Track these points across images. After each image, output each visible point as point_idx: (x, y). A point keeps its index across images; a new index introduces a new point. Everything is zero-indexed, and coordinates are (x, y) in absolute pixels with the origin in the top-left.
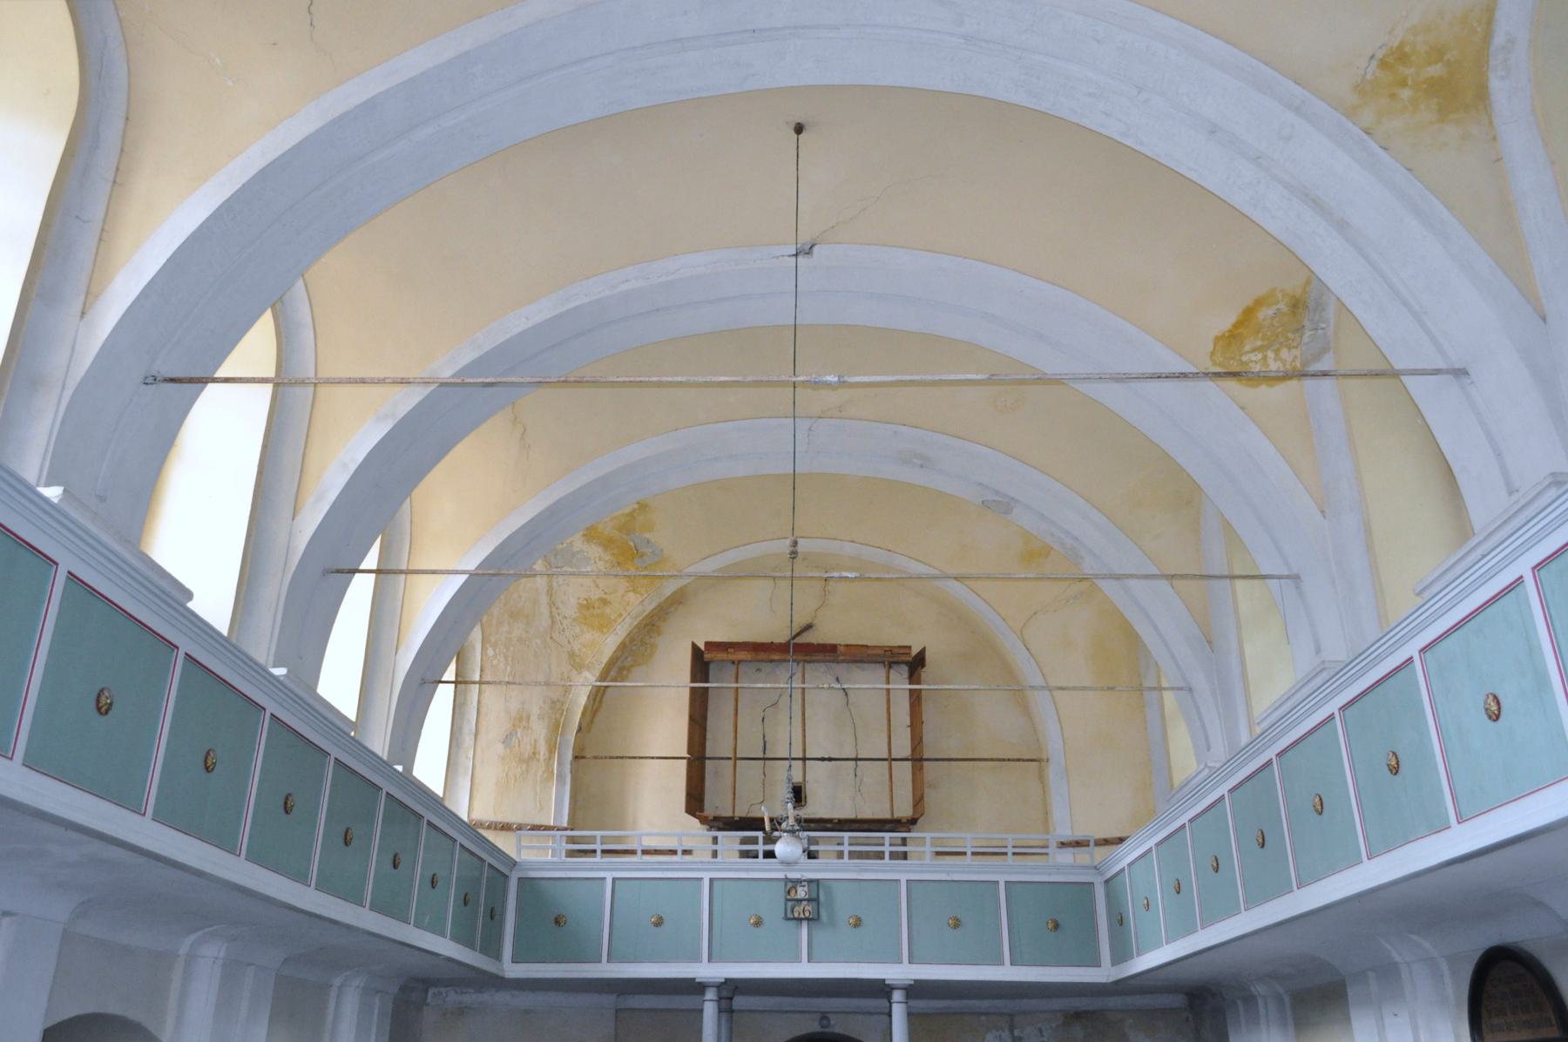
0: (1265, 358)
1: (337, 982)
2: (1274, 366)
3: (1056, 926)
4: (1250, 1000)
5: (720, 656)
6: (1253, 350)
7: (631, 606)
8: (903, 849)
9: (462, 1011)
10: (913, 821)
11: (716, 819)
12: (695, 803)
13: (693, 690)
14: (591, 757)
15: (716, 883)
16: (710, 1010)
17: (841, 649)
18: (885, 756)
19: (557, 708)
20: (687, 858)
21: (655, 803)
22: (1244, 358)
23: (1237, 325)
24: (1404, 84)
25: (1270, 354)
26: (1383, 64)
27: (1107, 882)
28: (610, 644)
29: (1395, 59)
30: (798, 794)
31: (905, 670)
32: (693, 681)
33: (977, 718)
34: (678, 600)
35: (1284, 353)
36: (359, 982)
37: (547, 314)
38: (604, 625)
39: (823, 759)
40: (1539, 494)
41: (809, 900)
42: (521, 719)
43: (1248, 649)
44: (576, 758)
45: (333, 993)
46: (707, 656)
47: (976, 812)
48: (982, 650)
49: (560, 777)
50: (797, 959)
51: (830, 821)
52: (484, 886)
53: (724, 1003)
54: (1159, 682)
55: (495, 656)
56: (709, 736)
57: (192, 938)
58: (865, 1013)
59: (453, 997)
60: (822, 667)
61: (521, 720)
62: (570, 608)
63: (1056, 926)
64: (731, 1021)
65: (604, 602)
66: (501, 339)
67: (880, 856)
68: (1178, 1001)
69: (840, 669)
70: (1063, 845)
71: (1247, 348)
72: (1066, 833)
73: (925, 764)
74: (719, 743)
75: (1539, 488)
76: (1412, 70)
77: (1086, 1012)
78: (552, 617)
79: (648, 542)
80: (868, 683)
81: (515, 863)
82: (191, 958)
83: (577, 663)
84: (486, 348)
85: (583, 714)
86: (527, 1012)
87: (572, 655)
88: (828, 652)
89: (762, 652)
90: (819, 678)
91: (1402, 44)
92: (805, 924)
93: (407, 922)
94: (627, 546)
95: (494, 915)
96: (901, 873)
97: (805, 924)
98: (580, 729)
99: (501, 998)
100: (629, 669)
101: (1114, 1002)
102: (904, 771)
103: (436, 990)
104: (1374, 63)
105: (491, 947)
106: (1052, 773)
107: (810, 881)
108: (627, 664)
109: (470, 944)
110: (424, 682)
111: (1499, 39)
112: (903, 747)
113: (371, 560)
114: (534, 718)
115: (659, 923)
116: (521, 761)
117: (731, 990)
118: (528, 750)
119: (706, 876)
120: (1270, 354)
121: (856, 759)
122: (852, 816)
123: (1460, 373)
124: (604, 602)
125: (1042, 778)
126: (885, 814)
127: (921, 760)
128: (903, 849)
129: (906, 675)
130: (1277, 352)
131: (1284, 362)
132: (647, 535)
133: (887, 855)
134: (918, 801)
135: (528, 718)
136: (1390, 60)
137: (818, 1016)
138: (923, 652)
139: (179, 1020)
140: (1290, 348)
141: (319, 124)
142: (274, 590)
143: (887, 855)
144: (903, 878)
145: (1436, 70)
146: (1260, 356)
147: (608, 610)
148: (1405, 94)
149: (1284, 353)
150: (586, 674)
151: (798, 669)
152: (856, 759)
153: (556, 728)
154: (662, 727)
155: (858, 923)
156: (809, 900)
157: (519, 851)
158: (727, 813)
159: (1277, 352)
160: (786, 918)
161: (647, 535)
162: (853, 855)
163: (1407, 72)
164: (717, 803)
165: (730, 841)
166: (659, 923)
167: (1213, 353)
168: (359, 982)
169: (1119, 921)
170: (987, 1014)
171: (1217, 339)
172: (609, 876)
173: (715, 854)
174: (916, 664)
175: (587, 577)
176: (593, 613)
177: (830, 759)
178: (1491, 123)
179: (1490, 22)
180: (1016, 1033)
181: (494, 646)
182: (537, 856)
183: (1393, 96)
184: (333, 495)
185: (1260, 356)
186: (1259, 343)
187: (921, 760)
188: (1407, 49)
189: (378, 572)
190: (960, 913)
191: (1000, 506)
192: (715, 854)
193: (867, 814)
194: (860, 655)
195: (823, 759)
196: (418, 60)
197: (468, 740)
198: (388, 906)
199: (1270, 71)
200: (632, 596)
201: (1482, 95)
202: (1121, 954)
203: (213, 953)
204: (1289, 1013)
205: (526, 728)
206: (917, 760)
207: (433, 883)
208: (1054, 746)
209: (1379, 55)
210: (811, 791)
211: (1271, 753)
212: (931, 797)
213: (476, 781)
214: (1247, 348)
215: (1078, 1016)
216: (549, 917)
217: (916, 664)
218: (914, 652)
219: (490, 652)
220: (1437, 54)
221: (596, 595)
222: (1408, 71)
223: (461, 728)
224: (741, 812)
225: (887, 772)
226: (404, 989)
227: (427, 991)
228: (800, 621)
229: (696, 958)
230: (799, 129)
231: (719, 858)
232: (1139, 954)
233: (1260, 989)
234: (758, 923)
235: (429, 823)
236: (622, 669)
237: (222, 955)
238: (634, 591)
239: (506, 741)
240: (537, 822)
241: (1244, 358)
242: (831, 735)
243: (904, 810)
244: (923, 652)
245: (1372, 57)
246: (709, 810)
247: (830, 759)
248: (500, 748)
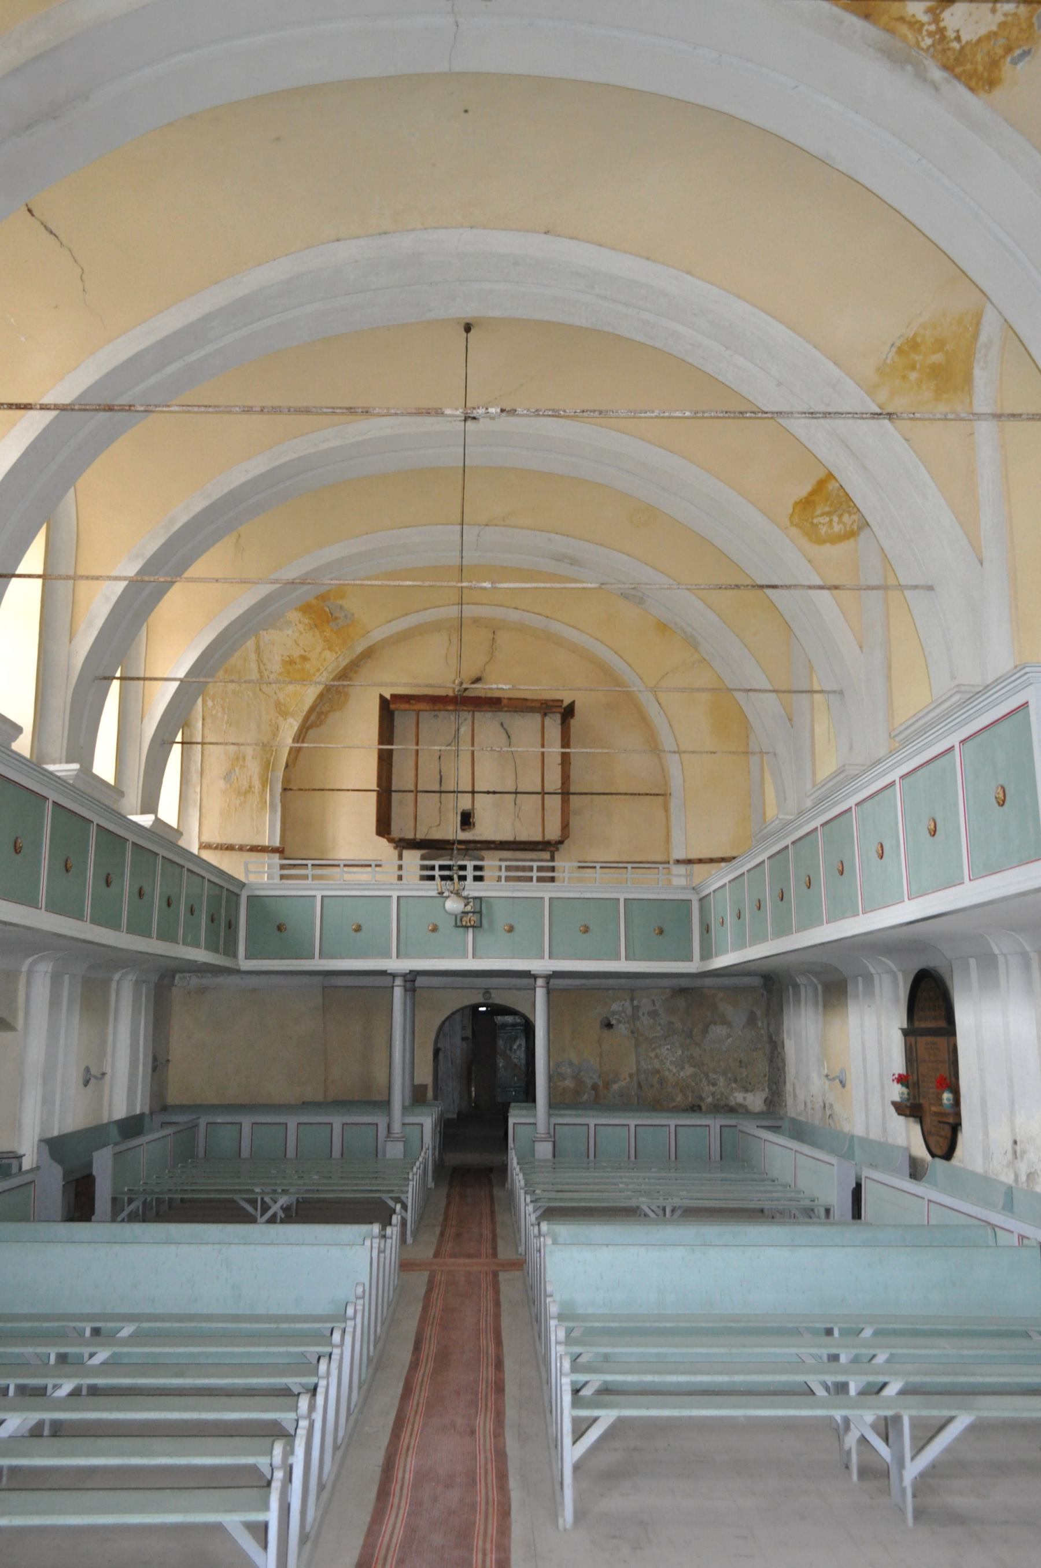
0: (831, 520)
1: (117, 976)
2: (837, 528)
3: (661, 932)
4: (796, 986)
5: (403, 706)
6: (822, 515)
7: (327, 663)
8: (551, 874)
9: (203, 990)
10: (561, 842)
11: (401, 840)
12: (383, 827)
13: (380, 751)
14: (297, 787)
15: (402, 900)
16: (398, 992)
17: (505, 702)
18: (539, 790)
19: (267, 749)
20: (377, 869)
21: (350, 825)
22: (815, 521)
23: (813, 493)
24: (913, 368)
25: (835, 518)
26: (900, 351)
27: (700, 900)
28: (310, 694)
29: (910, 347)
30: (467, 820)
31: (558, 718)
32: (381, 742)
33: (614, 756)
34: (368, 654)
35: (846, 518)
36: (131, 977)
37: (262, 469)
38: (304, 679)
39: (488, 793)
40: (951, 696)
41: (474, 913)
42: (238, 759)
43: (816, 726)
44: (285, 790)
45: (114, 985)
46: (392, 706)
47: (612, 830)
48: (624, 702)
49: (273, 806)
50: (465, 956)
51: (493, 842)
52: (221, 907)
53: (408, 985)
54: (668, 853)
55: (214, 706)
56: (394, 770)
57: (30, 960)
58: (517, 989)
59: (195, 981)
60: (490, 715)
61: (238, 760)
62: (275, 665)
63: (661, 932)
64: (413, 999)
65: (304, 659)
66: (226, 490)
67: (530, 879)
68: (757, 981)
69: (504, 717)
70: (678, 862)
71: (818, 512)
72: (682, 855)
73: (571, 797)
74: (402, 778)
75: (949, 694)
76: (921, 357)
77: (688, 989)
78: (260, 672)
79: (341, 607)
80: (526, 726)
81: (243, 885)
82: (30, 973)
83: (282, 711)
84: (214, 498)
85: (289, 753)
86: (254, 990)
87: (278, 704)
88: (493, 704)
89: (437, 702)
90: (488, 727)
91: (915, 336)
92: (471, 930)
93: (177, 942)
94: (324, 611)
95: (231, 926)
96: (546, 892)
97: (471, 930)
98: (287, 766)
99: (234, 979)
100: (326, 714)
101: (708, 982)
102: (554, 803)
103: (181, 975)
104: (894, 349)
105: (231, 951)
106: (673, 804)
107: (475, 898)
108: (324, 709)
109: (216, 950)
110: (163, 743)
111: (983, 338)
112: (554, 782)
113: (179, 738)
114: (249, 758)
115: (358, 929)
116: (239, 793)
117: (411, 978)
118: (244, 784)
119: (395, 894)
120: (835, 518)
121: (516, 793)
122: (511, 839)
123: (930, 588)
124: (304, 659)
125: (666, 809)
126: (538, 838)
127: (569, 793)
128: (551, 874)
129: (559, 721)
130: (840, 516)
131: (845, 525)
132: (340, 602)
133: (535, 879)
134: (565, 826)
135: (244, 758)
136: (906, 348)
137: (482, 992)
138: (573, 704)
139: (27, 1015)
140: (850, 513)
141: (97, 377)
142: (61, 700)
143: (535, 879)
144: (547, 896)
145: (937, 358)
146: (827, 519)
147: (307, 666)
148: (913, 376)
149: (846, 518)
150: (291, 720)
151: (468, 715)
152: (516, 793)
153: (267, 767)
154: (354, 763)
155: (511, 929)
156: (474, 913)
157: (247, 875)
158: (410, 836)
159: (840, 516)
160: (456, 926)
161: (340, 602)
162: (508, 879)
163: (917, 358)
164: (402, 827)
165: (413, 859)
166: (358, 929)
167: (792, 516)
168: (131, 977)
169: (706, 929)
170: (614, 989)
171: (796, 504)
172: (319, 894)
173: (400, 878)
174: (568, 713)
175: (288, 638)
176: (295, 668)
177: (494, 793)
178: (971, 403)
179: (978, 324)
180: (635, 1003)
181: (213, 698)
182: (259, 875)
183: (904, 377)
184: (100, 622)
185: (827, 519)
186: (827, 509)
187: (569, 793)
188: (919, 340)
189: (182, 743)
190: (586, 922)
191: (635, 596)
192: (400, 878)
193: (523, 837)
194: (520, 706)
195: (488, 793)
196: (170, 321)
197: (195, 778)
198: (167, 935)
199: (818, 353)
200: (328, 654)
201: (968, 379)
202: (706, 955)
203: (43, 971)
204: (820, 998)
205: (242, 767)
206: (565, 793)
207: (192, 912)
208: (676, 784)
209: (898, 343)
210: (479, 818)
211: (788, 841)
212: (574, 822)
213: (204, 811)
214: (818, 512)
215: (682, 991)
216: (273, 925)
217: (568, 713)
218: (566, 703)
219: (210, 703)
220: (940, 344)
221: (296, 653)
222: (917, 358)
223: (188, 768)
224: (420, 836)
225: (540, 802)
226: (162, 977)
227: (174, 978)
228: (470, 671)
229: (387, 955)
230: (468, 328)
231: (404, 881)
232: (716, 956)
233: (801, 980)
234: (435, 929)
235: (188, 870)
236: (321, 713)
237: (50, 970)
238: (330, 649)
239: (227, 777)
240: (255, 843)
241: (815, 521)
242: (494, 775)
243: (553, 833)
244: (573, 704)
245: (893, 345)
246: (396, 833)
247: (494, 793)
248: (222, 784)
